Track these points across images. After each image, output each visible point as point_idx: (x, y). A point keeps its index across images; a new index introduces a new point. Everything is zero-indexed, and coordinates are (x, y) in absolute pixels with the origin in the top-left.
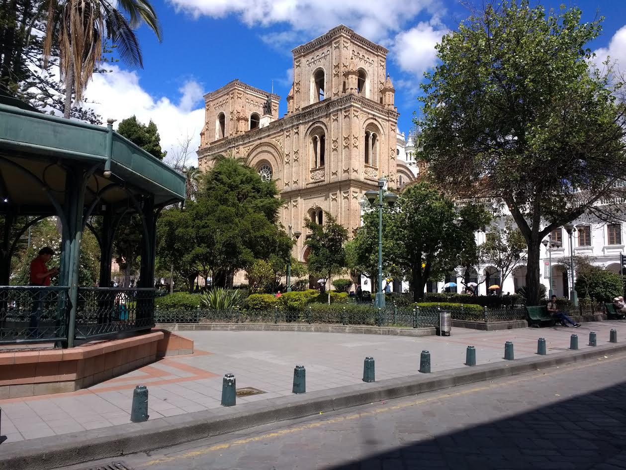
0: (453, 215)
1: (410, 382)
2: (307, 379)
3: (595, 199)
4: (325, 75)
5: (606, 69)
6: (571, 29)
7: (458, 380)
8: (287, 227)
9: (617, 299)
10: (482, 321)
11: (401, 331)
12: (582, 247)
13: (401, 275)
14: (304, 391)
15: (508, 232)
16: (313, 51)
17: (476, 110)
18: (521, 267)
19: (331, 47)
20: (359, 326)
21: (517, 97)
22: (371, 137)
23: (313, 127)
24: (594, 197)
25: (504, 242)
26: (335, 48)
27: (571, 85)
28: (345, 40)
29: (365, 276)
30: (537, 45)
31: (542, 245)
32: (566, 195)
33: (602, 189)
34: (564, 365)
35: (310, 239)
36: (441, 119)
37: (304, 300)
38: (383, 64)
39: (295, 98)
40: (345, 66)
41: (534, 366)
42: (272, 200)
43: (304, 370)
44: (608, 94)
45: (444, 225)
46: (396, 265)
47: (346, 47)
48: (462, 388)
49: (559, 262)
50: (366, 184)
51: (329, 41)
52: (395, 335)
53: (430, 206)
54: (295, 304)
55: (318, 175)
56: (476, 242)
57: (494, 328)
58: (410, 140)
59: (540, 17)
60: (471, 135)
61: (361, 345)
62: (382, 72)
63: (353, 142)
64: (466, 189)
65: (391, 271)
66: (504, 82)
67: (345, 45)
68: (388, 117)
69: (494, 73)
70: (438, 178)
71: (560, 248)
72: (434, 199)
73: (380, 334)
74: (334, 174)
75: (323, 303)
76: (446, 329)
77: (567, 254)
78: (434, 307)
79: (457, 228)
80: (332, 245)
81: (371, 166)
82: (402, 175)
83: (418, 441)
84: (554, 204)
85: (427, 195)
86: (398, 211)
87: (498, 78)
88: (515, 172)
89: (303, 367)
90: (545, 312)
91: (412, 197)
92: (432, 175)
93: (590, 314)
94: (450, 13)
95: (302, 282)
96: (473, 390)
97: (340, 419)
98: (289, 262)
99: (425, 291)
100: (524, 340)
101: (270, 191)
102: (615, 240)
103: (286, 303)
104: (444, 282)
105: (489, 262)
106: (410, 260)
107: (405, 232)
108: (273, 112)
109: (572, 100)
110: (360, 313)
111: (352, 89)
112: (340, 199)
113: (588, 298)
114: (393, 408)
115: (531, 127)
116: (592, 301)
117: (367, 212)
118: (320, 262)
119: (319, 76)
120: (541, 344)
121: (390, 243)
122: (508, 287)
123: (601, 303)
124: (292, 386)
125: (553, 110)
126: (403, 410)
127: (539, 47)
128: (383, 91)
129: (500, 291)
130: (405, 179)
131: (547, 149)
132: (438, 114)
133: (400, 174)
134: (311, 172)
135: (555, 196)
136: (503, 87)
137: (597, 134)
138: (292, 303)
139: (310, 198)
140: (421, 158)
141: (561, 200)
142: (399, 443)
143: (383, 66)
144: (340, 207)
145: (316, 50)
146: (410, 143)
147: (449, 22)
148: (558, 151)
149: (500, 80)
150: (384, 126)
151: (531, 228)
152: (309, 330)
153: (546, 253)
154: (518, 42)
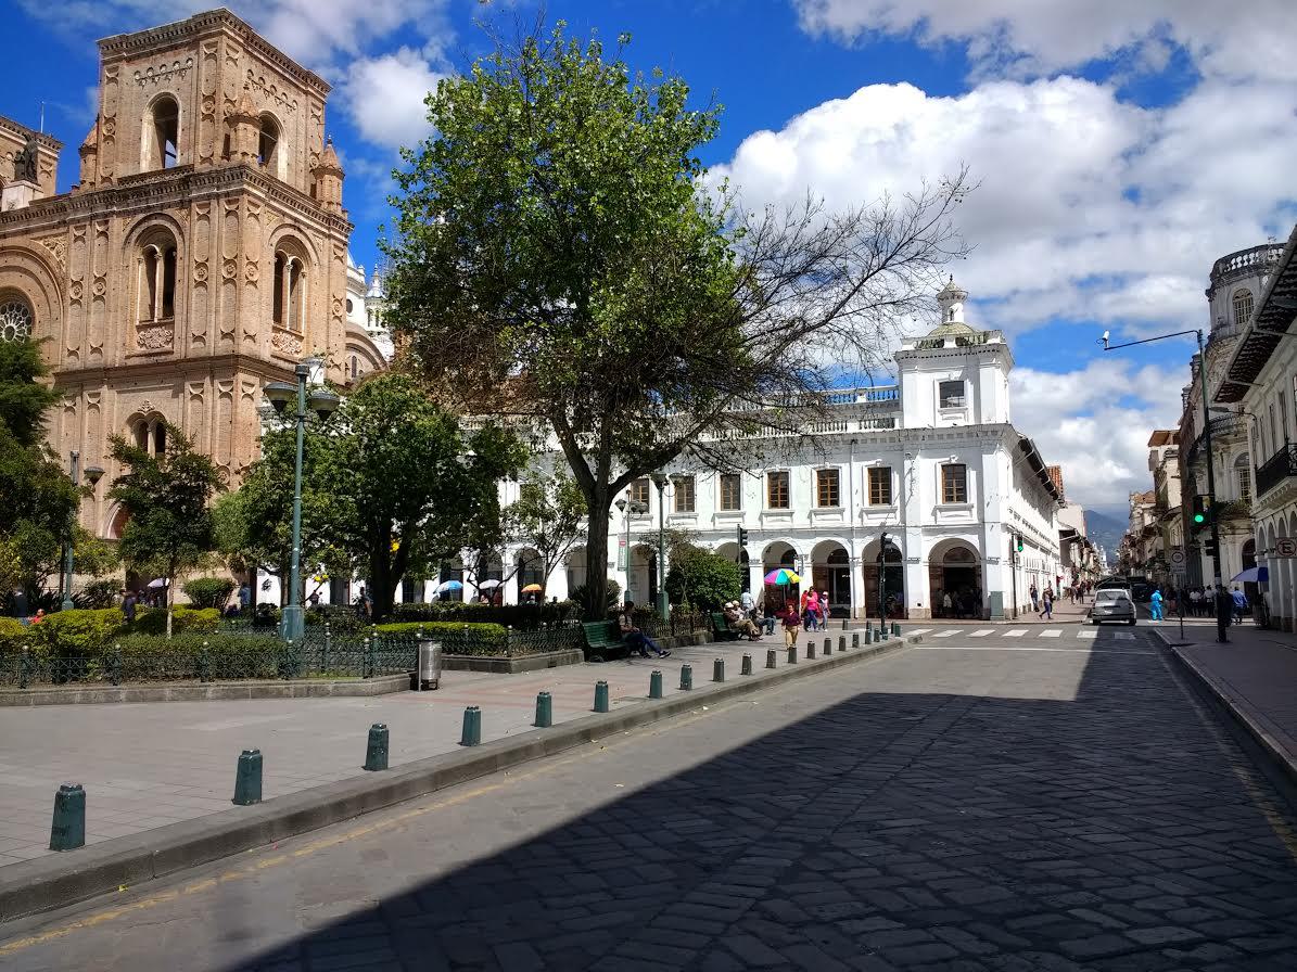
0: (458, 445)
1: (342, 793)
2: (50, 824)
3: (700, 429)
4: (180, 112)
5: (722, 200)
6: (670, 116)
7: (444, 778)
8: (65, 455)
9: (729, 605)
10: (502, 655)
11: (336, 688)
12: (679, 514)
13: (348, 568)
14: (81, 843)
15: (558, 482)
16: (152, 53)
17: (504, 242)
18: (577, 549)
19: (198, 53)
20: (240, 683)
21: (576, 228)
22: (289, 263)
23: (144, 226)
24: (698, 425)
25: (552, 503)
26: (208, 56)
27: (667, 220)
28: (231, 43)
29: (268, 571)
30: (613, 136)
31: (613, 508)
32: (654, 420)
33: (711, 412)
34: (637, 729)
35: (125, 487)
36: (435, 249)
37: (103, 628)
38: (319, 113)
39: (101, 152)
40: (231, 101)
41: (586, 735)
42: (28, 388)
43: (83, 796)
44: (725, 246)
45: (438, 465)
46: (336, 546)
47: (235, 61)
48: (450, 794)
49: (641, 539)
50: (274, 367)
51: (193, 37)
52: (322, 696)
53: (411, 425)
54: (79, 640)
55: (158, 338)
56: (499, 500)
57: (522, 668)
58: (377, 283)
59: (619, 83)
60: (493, 289)
61: (215, 729)
62: (317, 131)
63: (245, 270)
64: (482, 394)
65: (326, 560)
66: (553, 196)
67: (232, 54)
68: (329, 229)
69: (537, 174)
70: (428, 368)
71: (645, 515)
72: (419, 411)
73: (288, 696)
74: (197, 338)
75: (153, 633)
76: (430, 676)
77: (656, 526)
78: (412, 633)
79: (465, 471)
80: (182, 501)
81: (288, 329)
82: (359, 356)
83: (345, 916)
84: (635, 435)
85: (405, 402)
86: (343, 432)
87: (543, 186)
88: (569, 370)
89: (80, 787)
90: (613, 632)
91: (374, 404)
92: (415, 360)
93: (687, 632)
94: (461, 42)
95: (104, 586)
96: (470, 794)
97: (170, 896)
98: (69, 539)
99: (398, 597)
100: (571, 686)
101: (23, 366)
102: (881, 497)
103: (52, 638)
104: (437, 581)
105: (520, 539)
106: (365, 535)
107: (358, 476)
108: (41, 178)
109: (667, 248)
110: (248, 654)
111: (244, 154)
112: (210, 399)
113: (685, 605)
114: (299, 853)
115: (599, 288)
116: (692, 609)
117: (273, 428)
118: (148, 540)
119: (166, 112)
120: (601, 691)
121: (323, 500)
122: (557, 588)
123: (705, 611)
124: (48, 835)
125: (636, 261)
126: (320, 854)
127: (615, 140)
128: (318, 172)
129: (540, 595)
130: (365, 366)
131: (624, 332)
132: (429, 239)
133: (354, 354)
134: (139, 328)
135: (637, 419)
136: (553, 205)
137: (704, 315)
138: (68, 638)
139: (133, 391)
140: (397, 322)
141: (647, 426)
142: (301, 928)
143: (318, 118)
144: (210, 414)
145: (160, 51)
146: (377, 291)
147: (458, 57)
148: (641, 338)
149: (547, 191)
150: (320, 248)
151: (595, 478)
152: (111, 699)
153: (623, 524)
154: (580, 124)
